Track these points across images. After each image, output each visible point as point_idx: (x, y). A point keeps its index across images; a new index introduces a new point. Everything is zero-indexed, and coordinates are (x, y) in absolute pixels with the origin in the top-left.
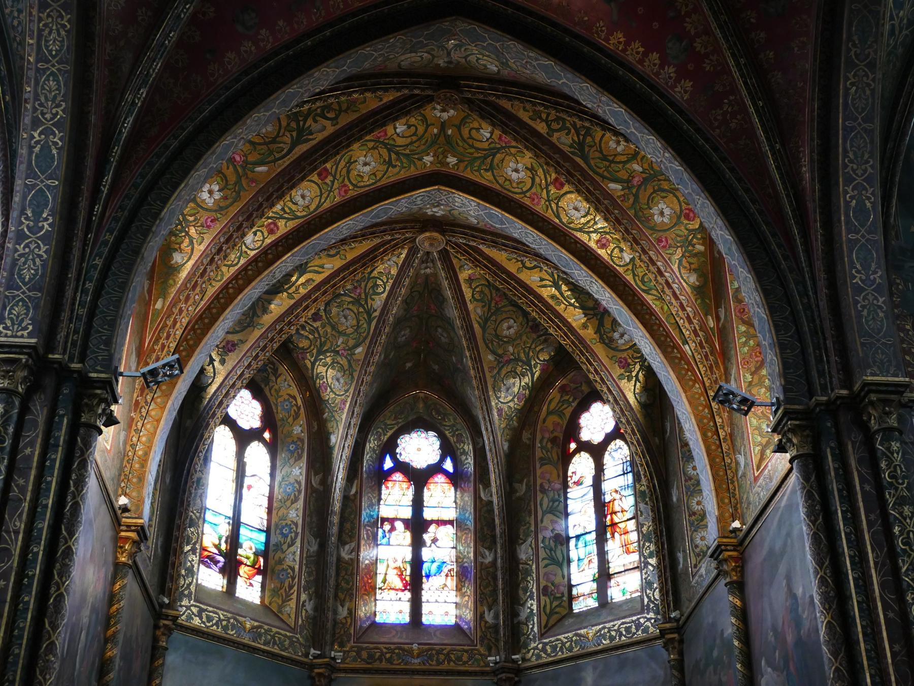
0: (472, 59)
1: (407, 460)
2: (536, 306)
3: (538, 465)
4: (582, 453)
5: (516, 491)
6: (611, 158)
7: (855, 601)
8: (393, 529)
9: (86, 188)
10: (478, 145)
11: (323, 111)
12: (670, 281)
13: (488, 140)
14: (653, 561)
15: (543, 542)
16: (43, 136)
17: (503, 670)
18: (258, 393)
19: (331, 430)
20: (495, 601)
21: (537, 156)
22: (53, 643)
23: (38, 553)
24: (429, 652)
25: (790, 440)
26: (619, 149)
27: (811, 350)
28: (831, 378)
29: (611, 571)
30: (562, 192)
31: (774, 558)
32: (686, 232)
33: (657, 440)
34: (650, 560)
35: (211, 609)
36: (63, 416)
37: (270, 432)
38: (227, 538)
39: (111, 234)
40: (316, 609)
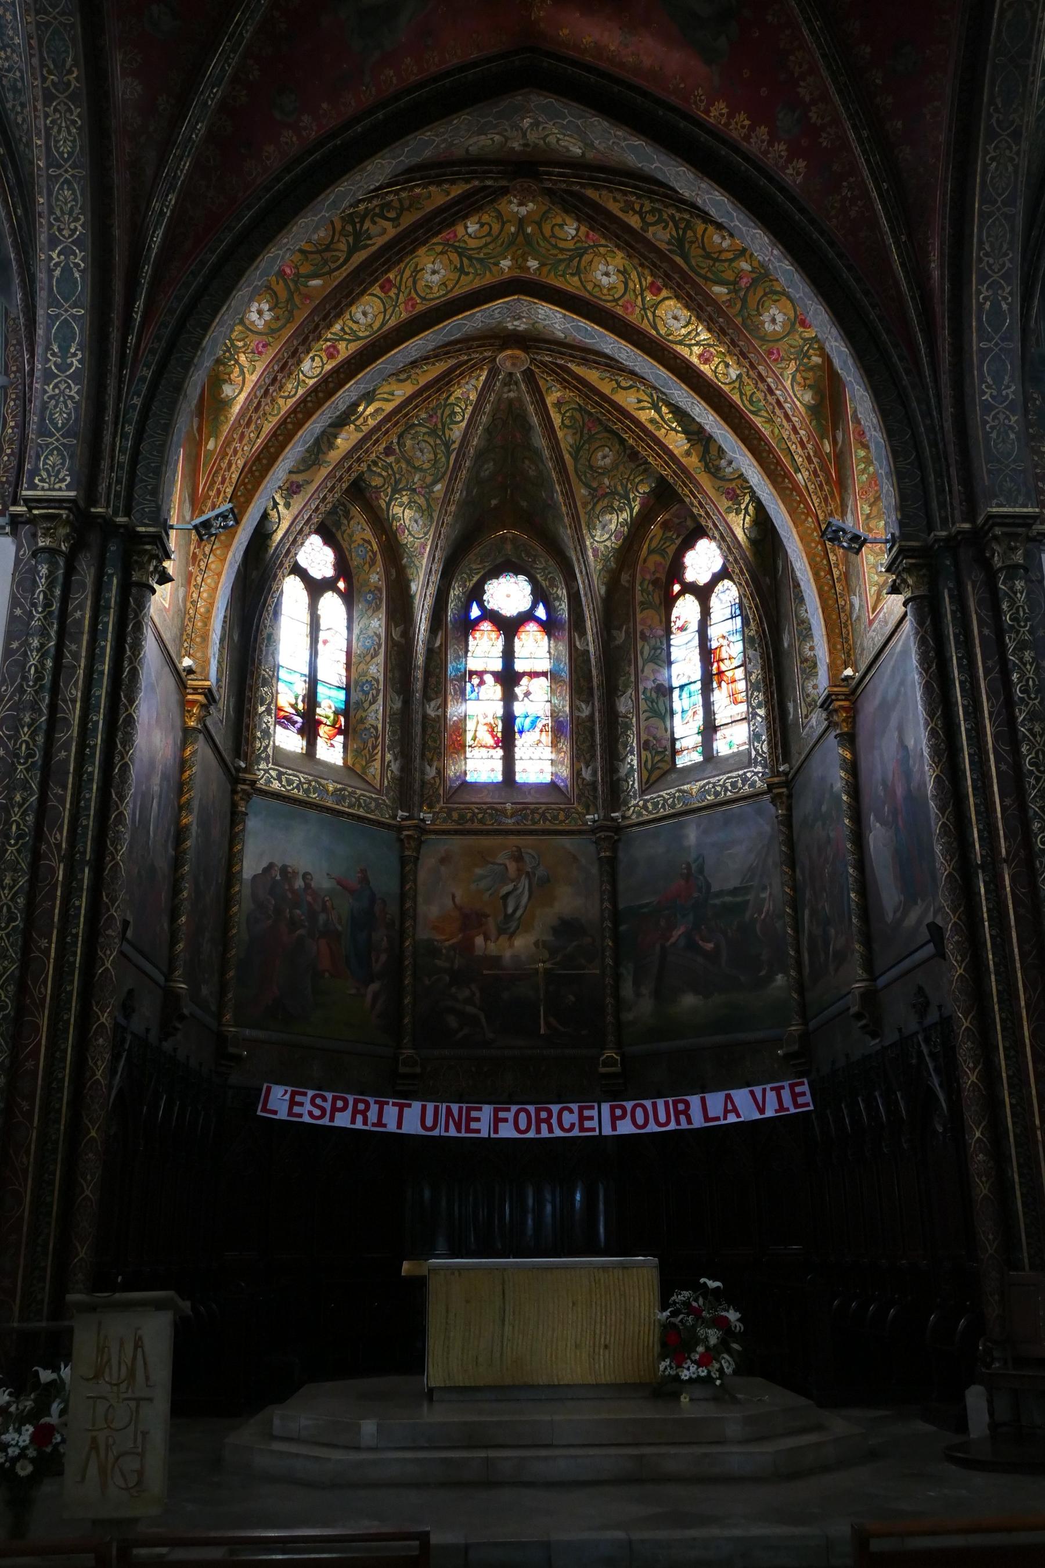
0: (552, 139)
1: (496, 608)
2: (633, 432)
3: (638, 610)
4: (687, 595)
5: (615, 639)
6: (715, 256)
7: (966, 753)
8: (482, 683)
9: (116, 316)
10: (562, 245)
11: (382, 211)
12: (782, 400)
13: (573, 238)
14: (761, 712)
15: (644, 693)
16: (62, 257)
17: (602, 828)
18: (329, 539)
19: (411, 577)
20: (593, 756)
21: (629, 256)
22: (121, 814)
23: (98, 721)
24: (523, 811)
25: (904, 581)
26: (725, 245)
27: (932, 478)
28: (953, 509)
29: (717, 723)
30: (660, 298)
31: (886, 708)
32: (801, 342)
33: (768, 580)
34: (758, 711)
35: (290, 772)
36: (112, 575)
37: (344, 581)
38: (304, 697)
39: (149, 368)
40: (402, 769)
